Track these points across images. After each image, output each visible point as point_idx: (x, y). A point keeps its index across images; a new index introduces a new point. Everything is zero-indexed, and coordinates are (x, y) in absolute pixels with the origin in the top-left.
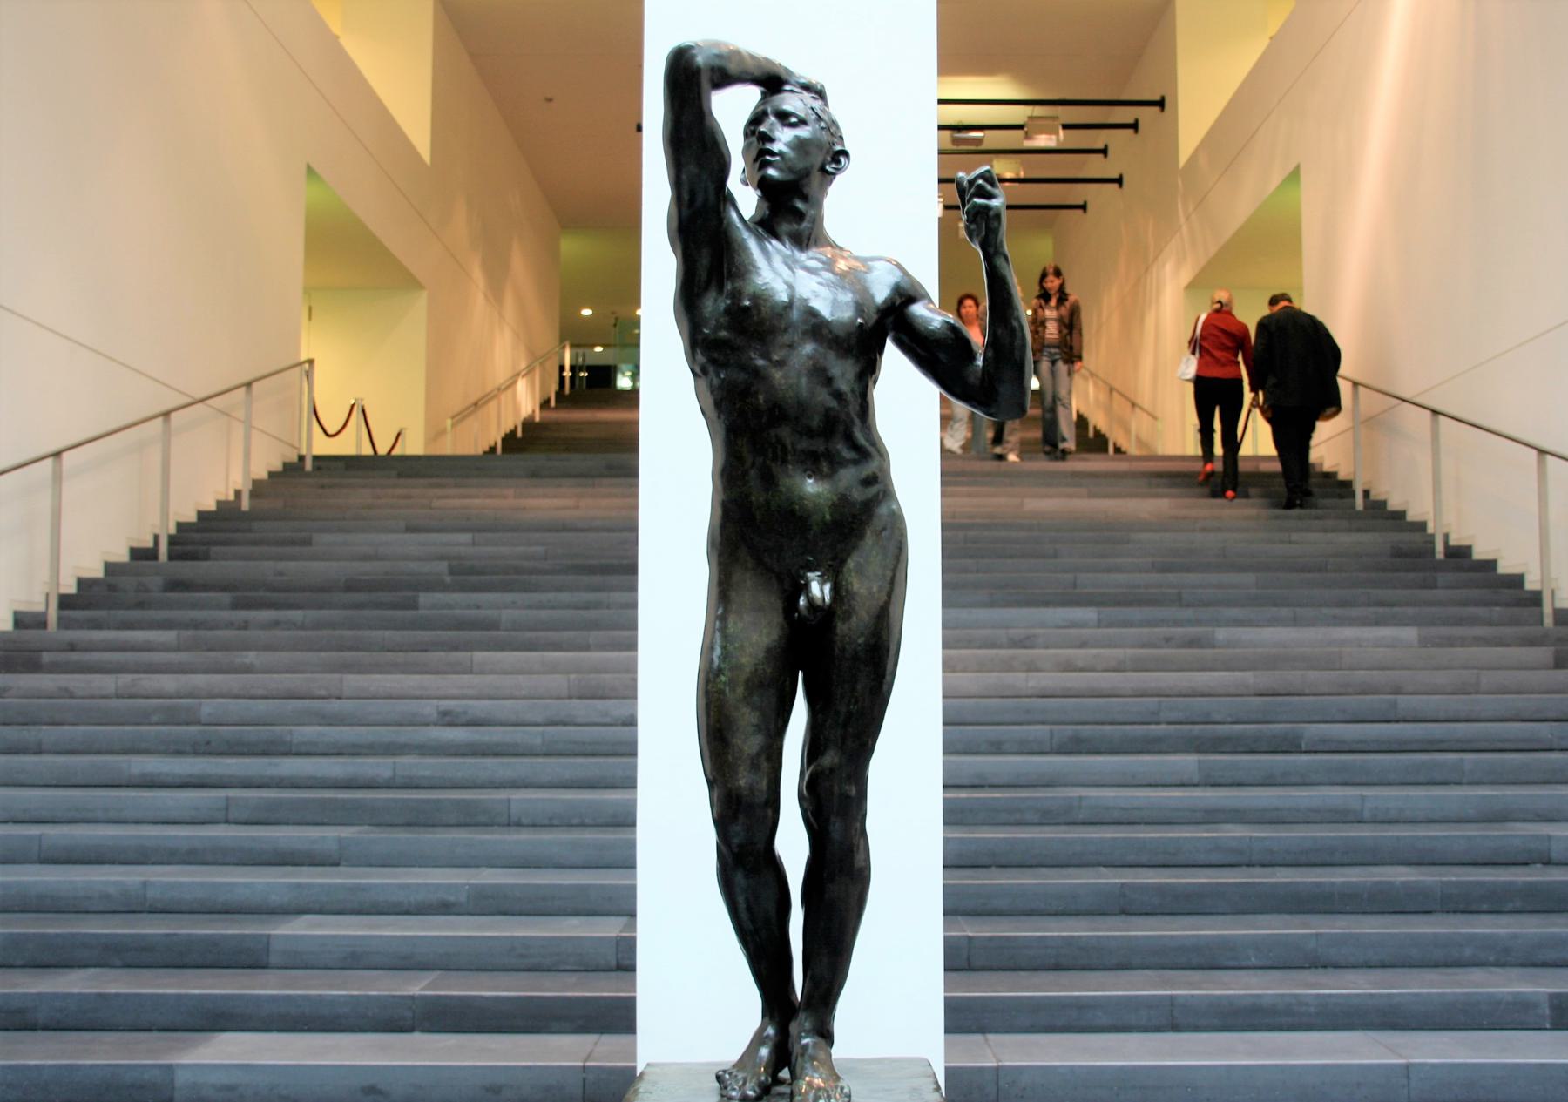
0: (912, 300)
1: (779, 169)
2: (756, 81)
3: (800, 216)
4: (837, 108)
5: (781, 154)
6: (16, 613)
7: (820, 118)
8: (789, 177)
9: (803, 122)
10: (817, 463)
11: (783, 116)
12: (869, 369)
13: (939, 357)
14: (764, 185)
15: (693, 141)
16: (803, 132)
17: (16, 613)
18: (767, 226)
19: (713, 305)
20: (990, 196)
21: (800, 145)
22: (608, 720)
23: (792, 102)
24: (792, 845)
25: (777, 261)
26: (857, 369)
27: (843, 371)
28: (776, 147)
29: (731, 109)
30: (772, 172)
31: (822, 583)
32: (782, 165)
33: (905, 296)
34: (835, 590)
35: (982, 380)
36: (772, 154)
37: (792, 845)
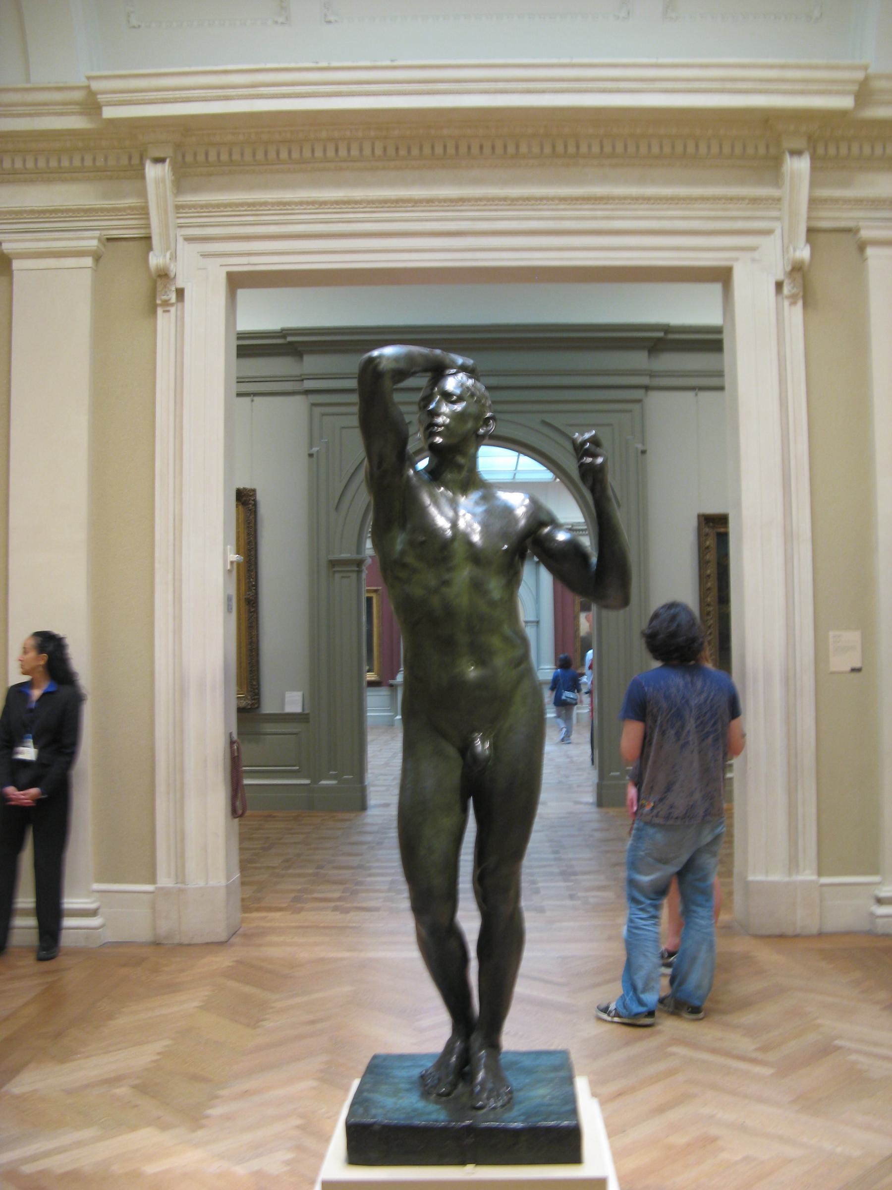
0: (543, 524)
2: (425, 370)
3: (460, 467)
6: (254, 491)
9: (460, 399)
10: (482, 657)
11: (447, 396)
12: (512, 579)
13: (564, 562)
16: (458, 407)
17: (254, 491)
18: (435, 475)
19: (400, 542)
20: (594, 456)
21: (458, 417)
22: (306, 924)
24: (469, 921)
25: (443, 502)
26: (503, 581)
27: (495, 586)
30: (439, 440)
31: (483, 743)
33: (540, 519)
34: (494, 746)
35: (597, 569)
36: (439, 426)
37: (469, 921)
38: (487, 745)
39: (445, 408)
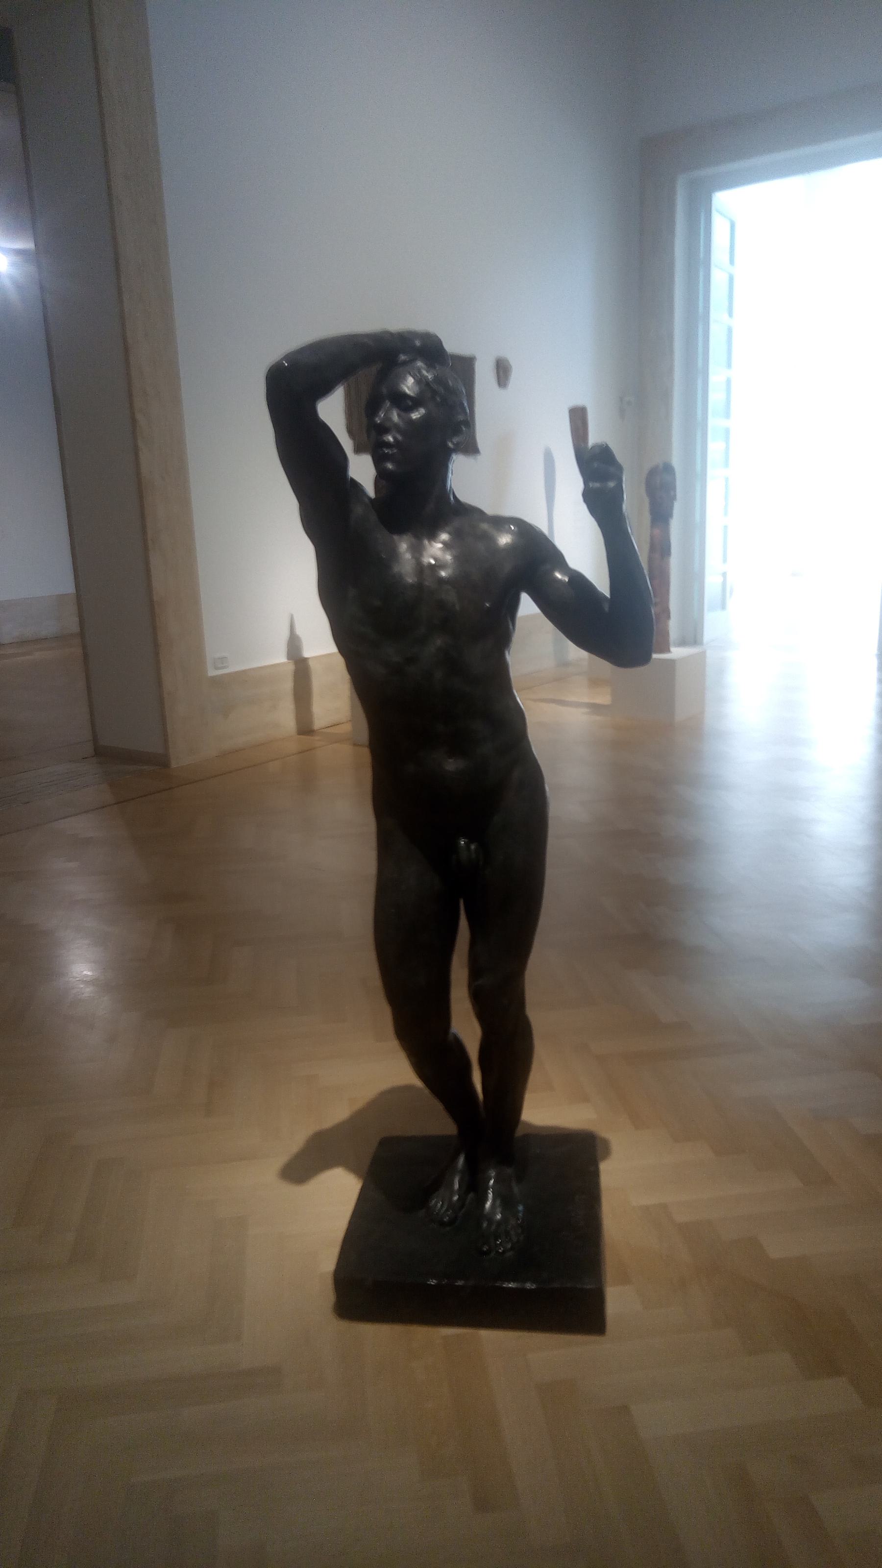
7: (434, 393)
9: (416, 403)
11: (403, 402)
15: (309, 459)
24: (466, 1028)
29: (332, 410)
30: (390, 466)
36: (388, 445)
37: (466, 1028)
38: (473, 847)
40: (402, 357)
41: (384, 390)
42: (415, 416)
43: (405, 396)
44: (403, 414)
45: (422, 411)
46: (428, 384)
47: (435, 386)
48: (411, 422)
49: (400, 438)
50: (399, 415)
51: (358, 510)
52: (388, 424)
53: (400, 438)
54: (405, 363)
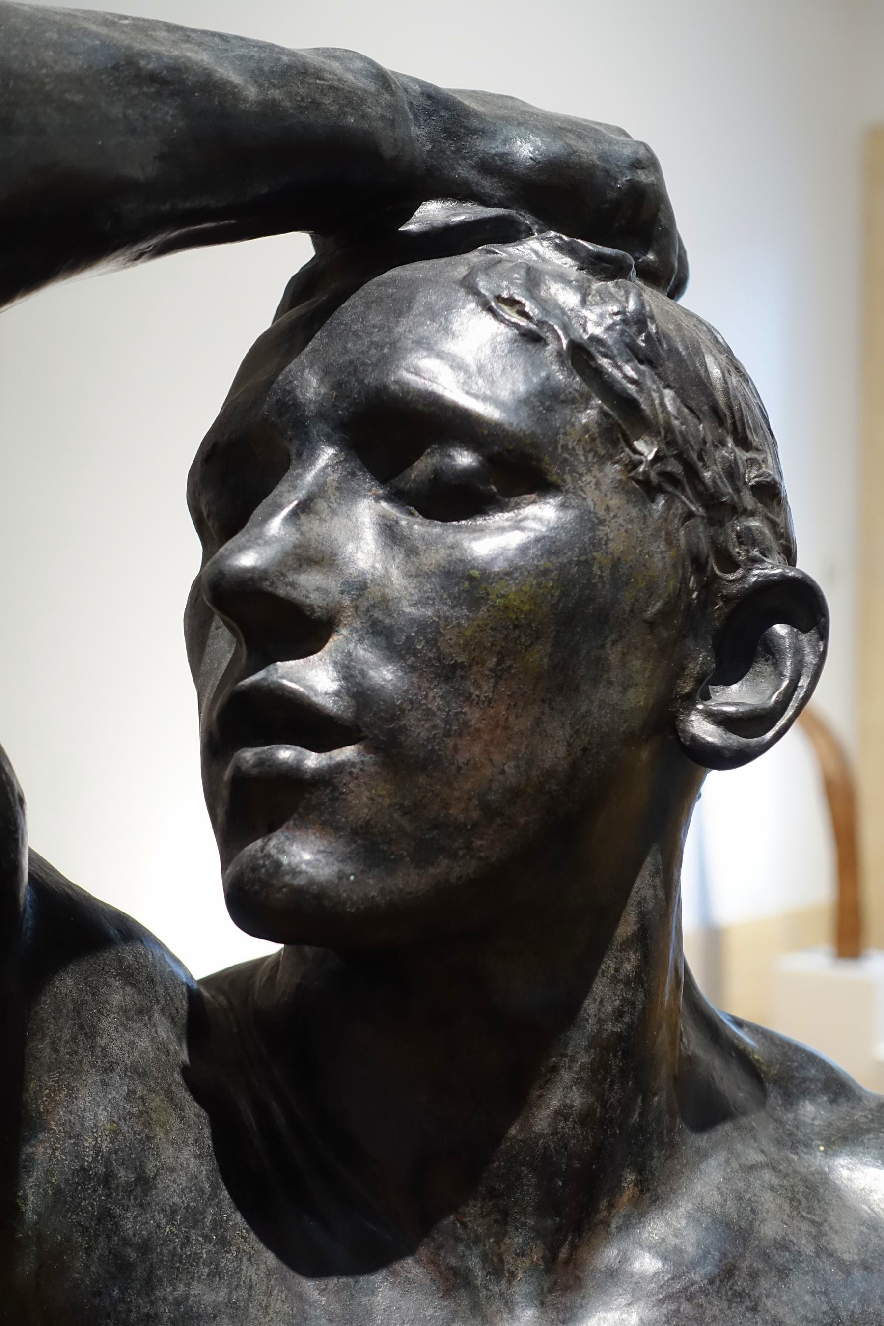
1: (367, 844)
4: (747, 301)
5: (359, 719)
7: (626, 416)
8: (408, 881)
9: (514, 468)
14: (251, 901)
23: (465, 356)
28: (315, 677)
32: (363, 801)
36: (305, 722)
39: (363, 536)
40: (433, 213)
41: (310, 385)
42: (499, 539)
43: (446, 423)
44: (416, 527)
45: (542, 515)
46: (580, 355)
47: (625, 372)
48: (467, 583)
49: (385, 675)
50: (390, 533)
51: (110, 1110)
52: (312, 587)
53: (385, 675)
54: (446, 242)
